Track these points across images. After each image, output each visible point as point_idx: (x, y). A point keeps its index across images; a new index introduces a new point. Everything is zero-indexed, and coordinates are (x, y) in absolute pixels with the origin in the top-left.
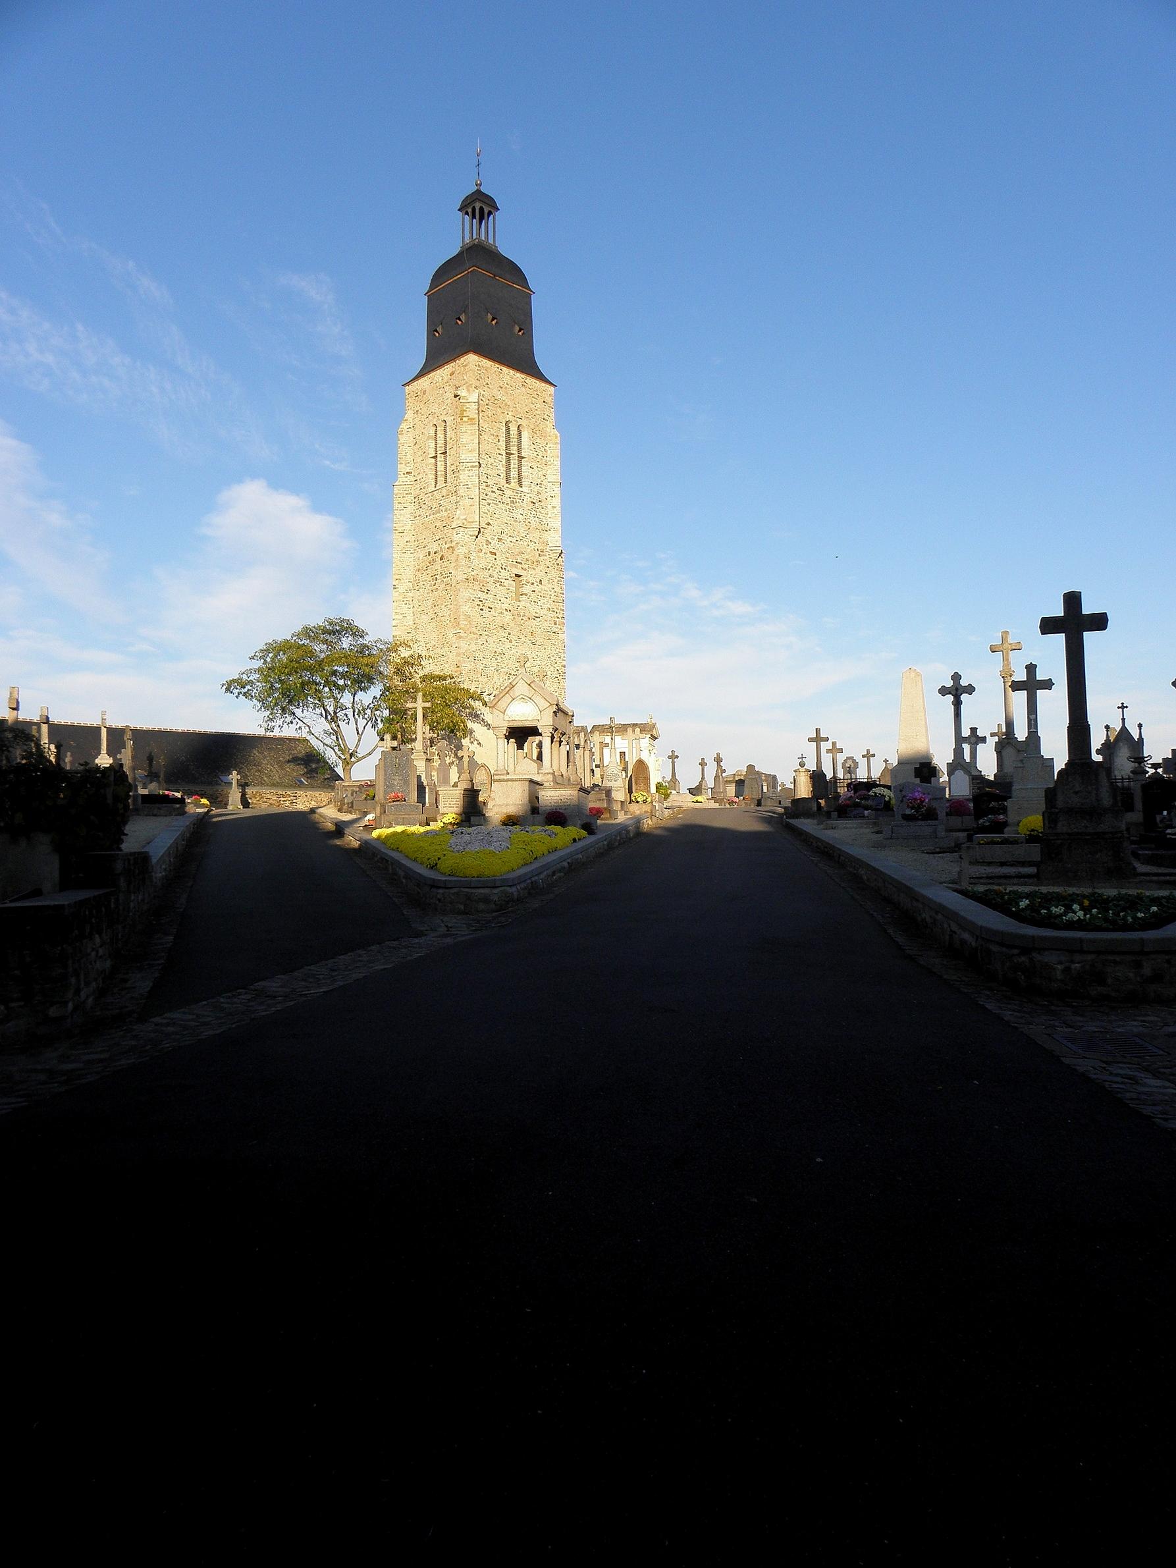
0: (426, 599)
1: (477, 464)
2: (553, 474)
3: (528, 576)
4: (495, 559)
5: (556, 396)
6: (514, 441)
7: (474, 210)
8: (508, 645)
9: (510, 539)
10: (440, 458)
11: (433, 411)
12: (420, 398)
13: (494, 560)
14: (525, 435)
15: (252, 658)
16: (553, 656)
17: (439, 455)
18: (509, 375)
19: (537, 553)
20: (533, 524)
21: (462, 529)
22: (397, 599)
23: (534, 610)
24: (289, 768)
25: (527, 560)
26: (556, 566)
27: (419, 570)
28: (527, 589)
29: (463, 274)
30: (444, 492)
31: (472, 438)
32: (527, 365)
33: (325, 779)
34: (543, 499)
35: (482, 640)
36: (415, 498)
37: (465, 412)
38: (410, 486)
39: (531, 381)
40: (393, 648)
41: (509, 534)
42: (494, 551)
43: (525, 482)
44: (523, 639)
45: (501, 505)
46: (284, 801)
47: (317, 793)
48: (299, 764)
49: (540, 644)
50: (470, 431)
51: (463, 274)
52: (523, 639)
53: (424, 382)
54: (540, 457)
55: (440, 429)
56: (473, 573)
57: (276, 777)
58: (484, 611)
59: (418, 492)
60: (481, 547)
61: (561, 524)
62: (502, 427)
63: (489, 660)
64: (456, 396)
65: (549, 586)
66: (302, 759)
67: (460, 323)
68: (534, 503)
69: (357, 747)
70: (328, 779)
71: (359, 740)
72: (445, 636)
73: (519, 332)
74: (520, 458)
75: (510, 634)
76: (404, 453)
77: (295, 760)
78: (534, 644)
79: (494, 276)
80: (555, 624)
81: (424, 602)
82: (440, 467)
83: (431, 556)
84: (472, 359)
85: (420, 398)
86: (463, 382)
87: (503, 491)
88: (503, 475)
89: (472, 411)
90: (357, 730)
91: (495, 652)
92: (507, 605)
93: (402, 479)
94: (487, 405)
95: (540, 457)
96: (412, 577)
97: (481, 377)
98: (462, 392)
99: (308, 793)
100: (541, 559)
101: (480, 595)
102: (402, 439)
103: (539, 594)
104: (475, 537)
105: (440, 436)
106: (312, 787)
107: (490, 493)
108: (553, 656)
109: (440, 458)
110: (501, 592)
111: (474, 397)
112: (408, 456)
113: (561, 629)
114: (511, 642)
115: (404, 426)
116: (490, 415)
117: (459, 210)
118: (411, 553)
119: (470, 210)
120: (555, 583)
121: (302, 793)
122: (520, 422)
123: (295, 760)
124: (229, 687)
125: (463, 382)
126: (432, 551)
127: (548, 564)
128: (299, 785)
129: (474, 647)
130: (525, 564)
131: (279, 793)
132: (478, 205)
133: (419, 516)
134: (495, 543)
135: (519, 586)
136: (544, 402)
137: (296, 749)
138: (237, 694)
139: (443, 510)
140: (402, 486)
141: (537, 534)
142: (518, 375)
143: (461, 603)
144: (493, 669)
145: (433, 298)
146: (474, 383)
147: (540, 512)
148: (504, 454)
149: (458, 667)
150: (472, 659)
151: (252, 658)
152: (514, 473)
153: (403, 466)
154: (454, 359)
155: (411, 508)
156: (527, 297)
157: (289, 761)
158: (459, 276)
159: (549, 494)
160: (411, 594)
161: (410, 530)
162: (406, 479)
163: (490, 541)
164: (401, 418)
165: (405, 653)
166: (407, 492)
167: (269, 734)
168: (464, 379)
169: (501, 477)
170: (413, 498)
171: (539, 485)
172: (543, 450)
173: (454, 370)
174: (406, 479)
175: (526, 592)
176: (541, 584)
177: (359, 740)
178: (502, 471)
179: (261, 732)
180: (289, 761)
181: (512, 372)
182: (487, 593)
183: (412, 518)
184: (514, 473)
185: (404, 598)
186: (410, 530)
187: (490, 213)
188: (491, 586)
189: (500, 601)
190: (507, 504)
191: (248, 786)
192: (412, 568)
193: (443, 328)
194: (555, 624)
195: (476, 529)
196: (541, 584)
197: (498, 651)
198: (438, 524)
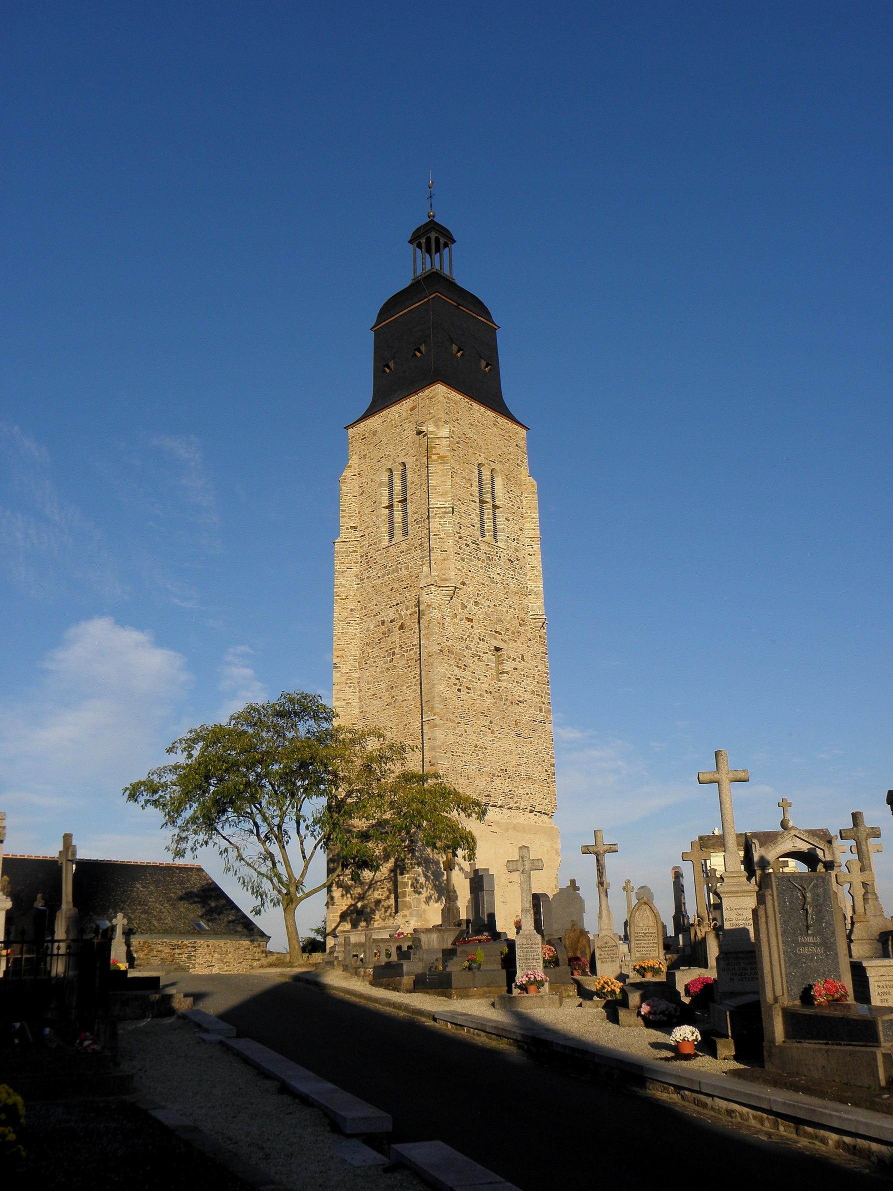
0: (378, 680)
1: (451, 509)
2: (531, 528)
3: (509, 649)
4: (472, 627)
5: (530, 441)
6: (487, 488)
7: (428, 240)
8: (490, 737)
9: (488, 603)
10: (398, 507)
11: (387, 453)
12: (369, 440)
13: (470, 628)
14: (499, 482)
15: (170, 750)
16: (541, 752)
17: (395, 504)
18: (479, 411)
19: (517, 622)
20: (512, 587)
21: (433, 588)
22: (339, 681)
23: (518, 692)
24: (183, 906)
25: (507, 630)
26: (538, 638)
27: (368, 644)
28: (508, 666)
29: (422, 302)
30: (404, 546)
31: (443, 479)
32: (495, 402)
33: (229, 922)
34: (520, 557)
35: (460, 729)
36: (362, 557)
37: (434, 450)
38: (356, 543)
39: (503, 421)
40: (359, 739)
41: (486, 598)
42: (470, 617)
43: (501, 536)
44: (506, 730)
45: (476, 562)
46: (180, 954)
47: (222, 943)
48: (195, 902)
49: (525, 736)
50: (441, 472)
51: (422, 302)
52: (506, 730)
53: (374, 422)
54: (515, 508)
55: (397, 474)
56: (448, 644)
57: (168, 921)
58: (462, 693)
59: (365, 549)
60: (456, 611)
61: (543, 588)
62: (474, 470)
63: (469, 755)
64: (419, 433)
65: (532, 663)
66: (197, 896)
67: (419, 354)
68: (512, 562)
69: (303, 875)
70: (233, 921)
71: (306, 867)
72: (408, 726)
73: (485, 368)
74: (495, 507)
75: (491, 722)
76: (347, 505)
77: (188, 897)
78: (519, 735)
79: (459, 304)
80: (541, 711)
81: (376, 684)
82: (398, 517)
83: (386, 625)
84: (440, 389)
85: (369, 440)
86: (429, 416)
87: (478, 545)
88: (478, 526)
89: (443, 447)
90: (303, 852)
91: (476, 746)
92: (487, 686)
93: (345, 534)
94: (458, 443)
95: (515, 508)
96: (358, 653)
97: (450, 412)
98: (429, 427)
99: (211, 942)
100: (522, 629)
101: (457, 671)
102: (344, 489)
103: (522, 673)
104: (450, 599)
105: (397, 482)
106: (215, 934)
107: (464, 547)
108: (541, 752)
109: (398, 507)
110: (479, 667)
111: (444, 432)
112: (353, 507)
113: (547, 717)
114: (493, 733)
115: (347, 473)
116: (461, 455)
117: (409, 242)
118: (357, 624)
119: (423, 241)
120: (538, 660)
121: (202, 942)
122: (493, 466)
123: (188, 897)
124: (133, 794)
125: (429, 416)
126: (387, 619)
127: (531, 636)
128: (198, 932)
129: (452, 739)
130: (505, 634)
131: (175, 942)
132: (433, 235)
133: (368, 578)
134: (471, 607)
135: (500, 662)
136: (517, 445)
137: (189, 882)
138: (143, 803)
139: (403, 569)
140: (345, 543)
141: (516, 599)
142: (489, 413)
143: (436, 682)
144: (474, 767)
145: (379, 333)
146: (442, 415)
147: (518, 573)
148: (477, 500)
149: (433, 765)
150: (449, 755)
151: (170, 750)
152: (488, 525)
153: (346, 519)
154: (415, 392)
155: (356, 569)
156: (492, 331)
157: (181, 898)
158: (417, 305)
159: (527, 552)
160: (356, 675)
161: (355, 596)
162: (350, 535)
163: (466, 604)
164: (344, 463)
165: (372, 745)
166: (351, 550)
167: (180, 862)
168: (430, 413)
169: (476, 528)
170: (358, 557)
171: (516, 541)
172: (519, 501)
173: (415, 404)
174: (350, 535)
175: (507, 669)
176: (523, 660)
177: (306, 867)
178: (476, 521)
179: (166, 859)
180: (181, 898)
181: (483, 409)
182: (464, 669)
183: (358, 581)
184: (488, 525)
185: (347, 680)
186: (355, 596)
187: (446, 245)
188: (469, 661)
189: (479, 680)
190: (483, 561)
191: (134, 934)
192: (357, 641)
193: (395, 363)
194: (541, 711)
195: (450, 589)
196: (523, 660)
197: (479, 743)
198: (396, 586)
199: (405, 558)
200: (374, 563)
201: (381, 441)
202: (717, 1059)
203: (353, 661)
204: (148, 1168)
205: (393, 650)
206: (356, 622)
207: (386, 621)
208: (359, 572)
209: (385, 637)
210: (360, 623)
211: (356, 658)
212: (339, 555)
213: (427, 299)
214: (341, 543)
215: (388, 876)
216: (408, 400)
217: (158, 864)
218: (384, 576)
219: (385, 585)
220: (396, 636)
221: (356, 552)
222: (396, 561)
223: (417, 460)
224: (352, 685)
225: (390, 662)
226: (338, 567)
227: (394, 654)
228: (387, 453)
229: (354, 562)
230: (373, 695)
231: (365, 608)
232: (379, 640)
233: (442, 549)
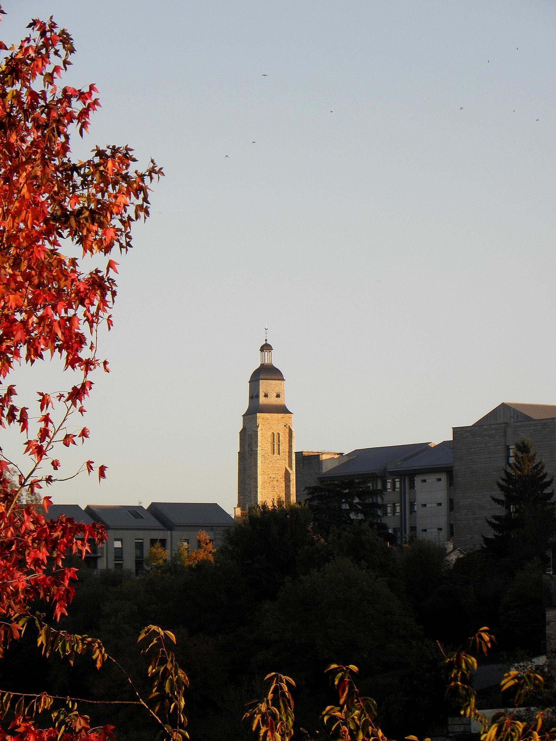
220: (275, 483)
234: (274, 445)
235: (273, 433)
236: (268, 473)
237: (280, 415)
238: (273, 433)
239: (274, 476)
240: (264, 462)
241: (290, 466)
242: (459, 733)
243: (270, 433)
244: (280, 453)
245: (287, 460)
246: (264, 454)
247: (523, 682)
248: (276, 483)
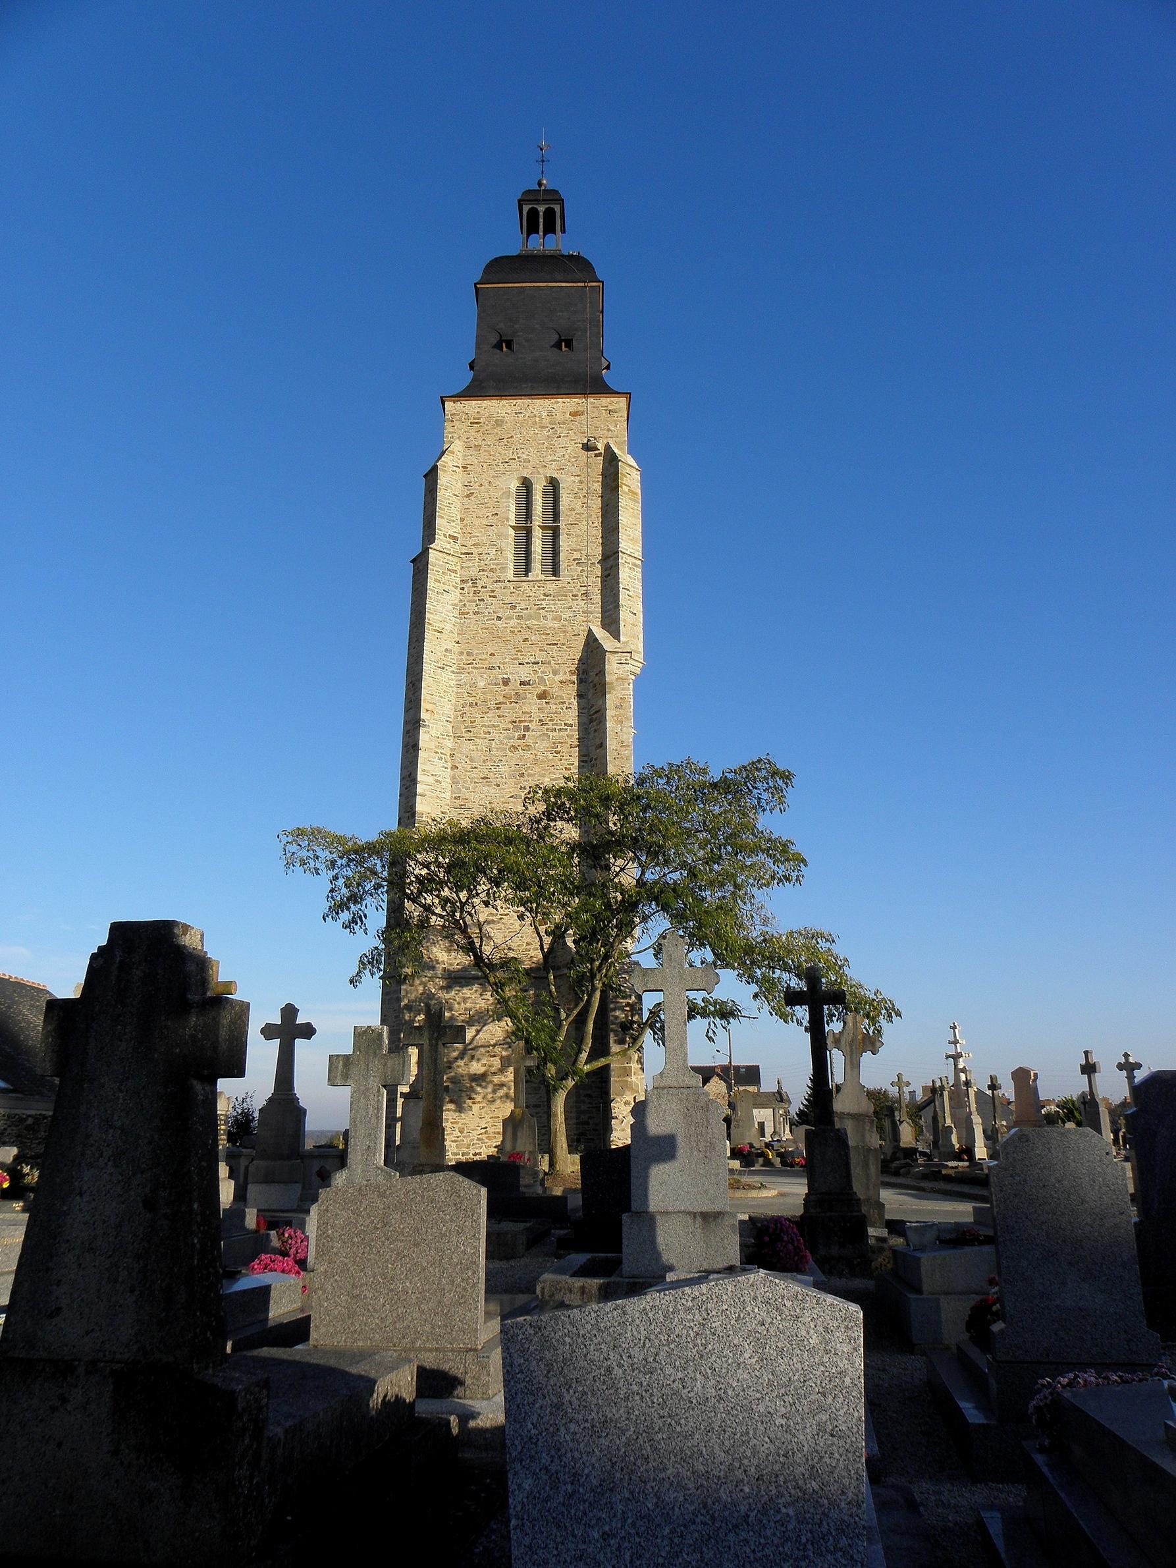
38: (456, 560)
51: (575, 285)
126: (515, 681)
161: (451, 632)
162: (448, 546)
174: (448, 546)
199: (554, 604)
200: (490, 596)
201: (512, 437)
202: (309, 1317)
203: (445, 724)
204: (289, 1518)
205: (526, 724)
206: (451, 669)
207: (512, 681)
208: (457, 601)
209: (511, 703)
210: (458, 673)
211: (450, 720)
212: (435, 569)
213: (583, 284)
214: (437, 553)
215: (504, 1040)
216: (568, 400)
217: (7, 977)
218: (509, 618)
219: (512, 632)
220: (532, 705)
221: (455, 572)
222: (535, 605)
223: (581, 482)
224: (443, 756)
225: (519, 739)
226: (433, 584)
227: (527, 729)
228: (524, 456)
229: (453, 586)
230: (483, 778)
231: (469, 654)
232: (496, 704)
233: (631, 610)
234: (528, 532)
235: (527, 484)
236: (496, 661)
237: (562, 406)
238: (527, 484)
239: (524, 673)
240: (471, 607)
241: (611, 621)
242: (265, 1409)
243: (514, 485)
244: (563, 566)
245: (597, 598)
246: (473, 573)
247: (507, 1319)
248: (534, 709)
